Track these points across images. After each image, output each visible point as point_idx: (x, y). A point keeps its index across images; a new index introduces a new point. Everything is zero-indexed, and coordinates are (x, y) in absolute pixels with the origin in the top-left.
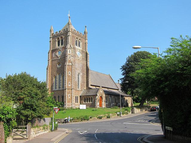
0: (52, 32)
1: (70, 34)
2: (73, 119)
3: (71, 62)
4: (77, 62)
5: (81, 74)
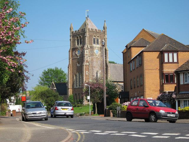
0: (72, 30)
1: (87, 34)
2: (85, 114)
3: (89, 62)
4: (95, 60)
5: (100, 71)
